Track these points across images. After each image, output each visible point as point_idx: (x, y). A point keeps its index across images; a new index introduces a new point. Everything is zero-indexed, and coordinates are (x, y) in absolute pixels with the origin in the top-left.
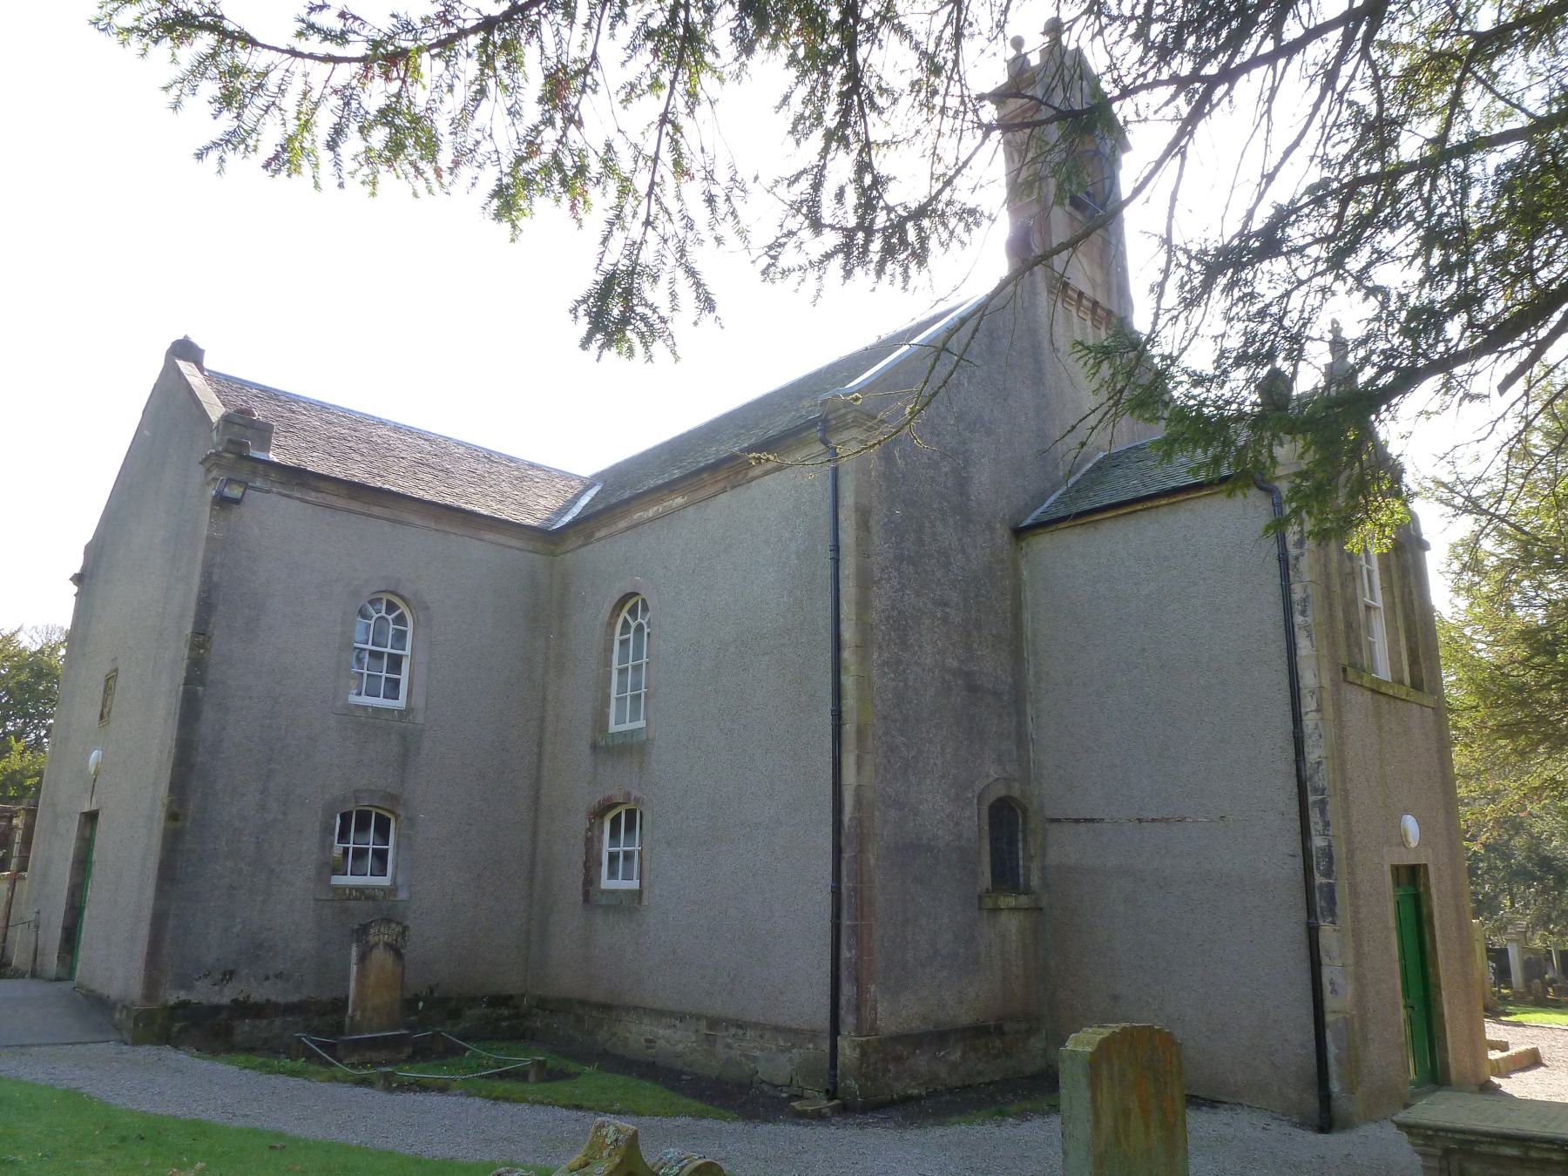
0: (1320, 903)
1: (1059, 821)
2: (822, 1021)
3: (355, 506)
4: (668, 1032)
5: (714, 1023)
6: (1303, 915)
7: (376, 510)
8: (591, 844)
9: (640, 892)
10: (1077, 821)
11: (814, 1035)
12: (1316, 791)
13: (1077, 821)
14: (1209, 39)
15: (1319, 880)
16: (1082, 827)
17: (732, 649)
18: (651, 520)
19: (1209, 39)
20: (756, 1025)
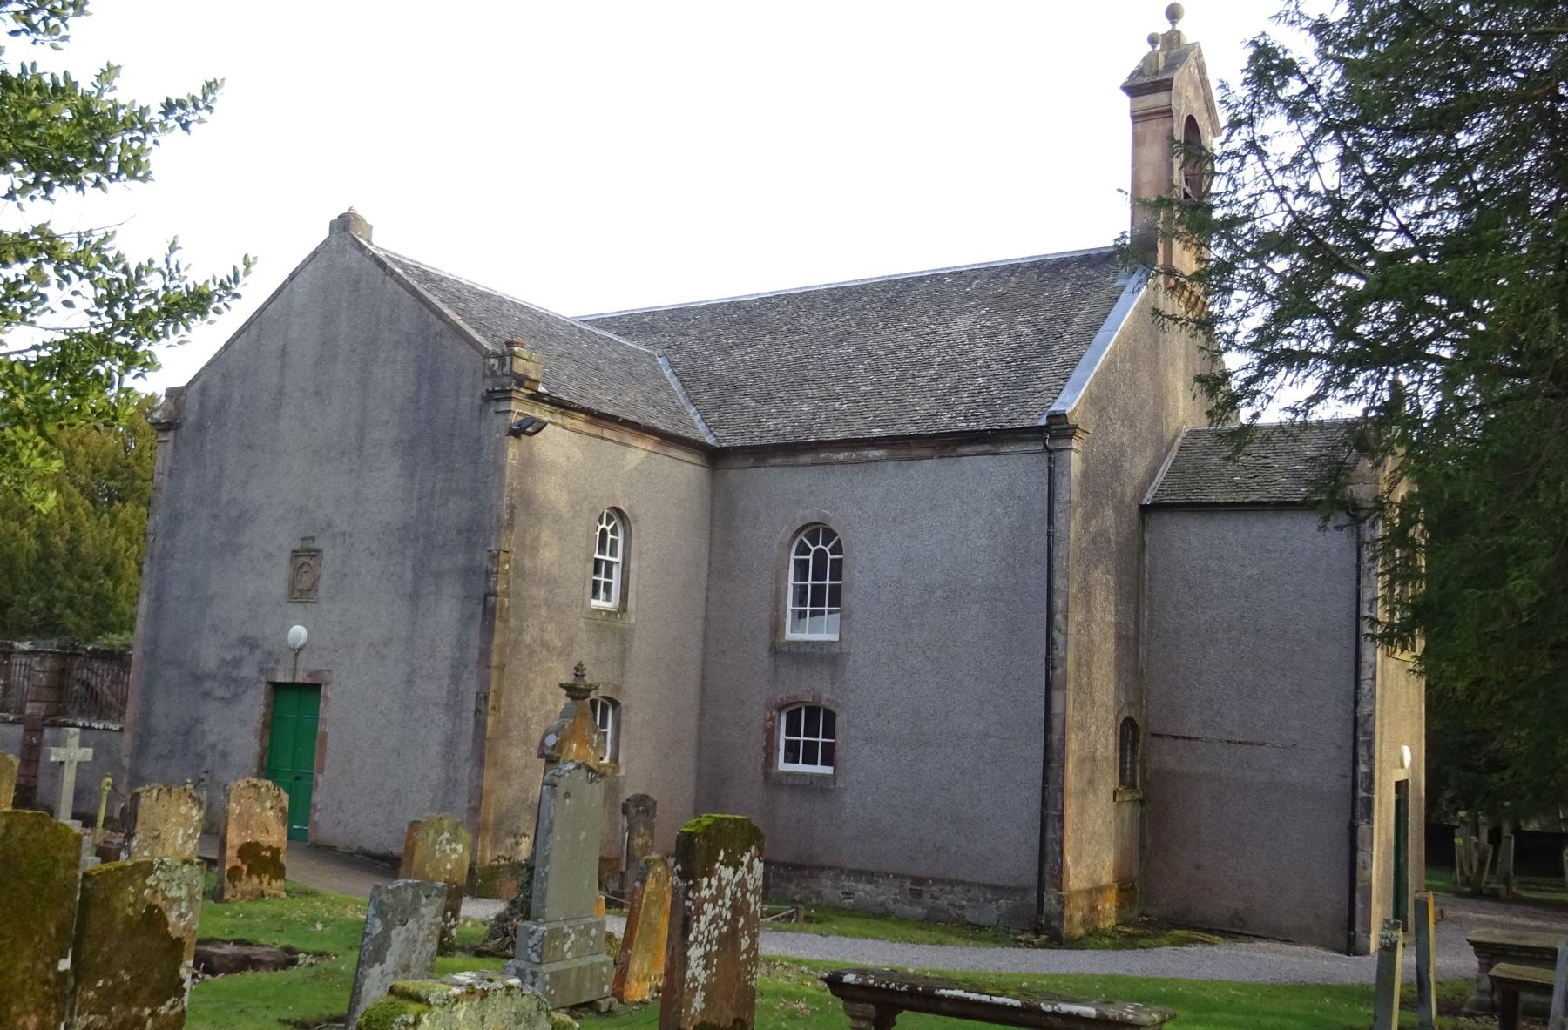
0: (1360, 808)
1: (1161, 736)
2: (1031, 878)
3: (595, 430)
4: (868, 887)
5: (919, 880)
6: (1349, 816)
7: (607, 433)
8: (771, 734)
9: (834, 777)
10: (1176, 738)
11: (1024, 890)
12: (1365, 734)
13: (1176, 738)
14: (1404, 585)
15: (1361, 793)
16: (1180, 742)
17: (939, 593)
18: (842, 463)
19: (1404, 585)
20: (963, 883)
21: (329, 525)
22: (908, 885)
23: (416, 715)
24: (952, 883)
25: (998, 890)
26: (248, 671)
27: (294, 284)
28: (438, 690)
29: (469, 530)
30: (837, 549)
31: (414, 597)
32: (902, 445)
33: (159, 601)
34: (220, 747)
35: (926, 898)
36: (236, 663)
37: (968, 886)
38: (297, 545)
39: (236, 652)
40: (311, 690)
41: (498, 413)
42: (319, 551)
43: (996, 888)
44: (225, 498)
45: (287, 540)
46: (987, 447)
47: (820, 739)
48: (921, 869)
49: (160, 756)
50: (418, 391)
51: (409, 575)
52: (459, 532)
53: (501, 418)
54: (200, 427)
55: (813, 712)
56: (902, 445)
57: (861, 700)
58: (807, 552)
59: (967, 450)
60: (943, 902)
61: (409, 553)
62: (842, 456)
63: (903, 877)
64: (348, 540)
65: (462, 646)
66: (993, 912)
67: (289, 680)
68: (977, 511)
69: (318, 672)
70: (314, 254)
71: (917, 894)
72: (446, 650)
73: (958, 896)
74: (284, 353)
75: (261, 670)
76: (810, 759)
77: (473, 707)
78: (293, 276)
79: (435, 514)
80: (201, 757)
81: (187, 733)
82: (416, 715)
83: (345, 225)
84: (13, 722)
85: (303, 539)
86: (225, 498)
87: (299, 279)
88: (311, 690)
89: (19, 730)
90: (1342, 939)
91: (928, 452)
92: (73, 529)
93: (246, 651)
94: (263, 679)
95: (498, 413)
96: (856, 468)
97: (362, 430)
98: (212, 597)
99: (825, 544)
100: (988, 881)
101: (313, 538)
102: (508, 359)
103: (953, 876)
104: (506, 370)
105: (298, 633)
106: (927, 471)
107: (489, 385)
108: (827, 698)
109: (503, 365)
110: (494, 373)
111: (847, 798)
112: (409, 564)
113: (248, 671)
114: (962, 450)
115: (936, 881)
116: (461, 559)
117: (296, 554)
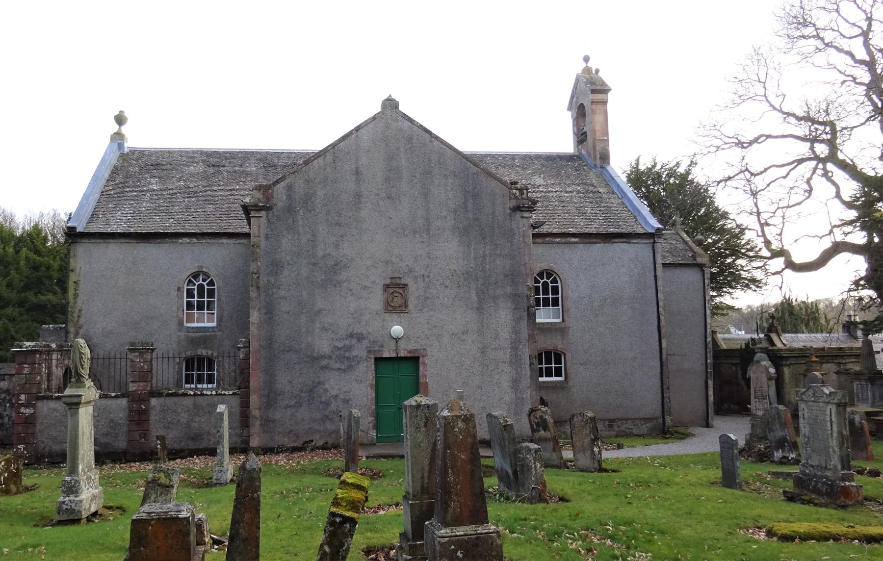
2: (659, 413)
11: (657, 418)
20: (629, 419)
21: (411, 271)
22: (607, 423)
23: (490, 369)
24: (626, 420)
25: (646, 420)
26: (360, 351)
27: (359, 133)
28: (505, 355)
29: (512, 275)
30: (555, 281)
31: (480, 309)
32: (586, 237)
33: (269, 312)
34: (341, 396)
35: (616, 428)
36: (348, 348)
37: (634, 419)
38: (388, 282)
39: (347, 342)
40: (414, 360)
41: (523, 217)
42: (406, 285)
43: (645, 419)
44: (320, 253)
45: (378, 278)
46: (625, 240)
47: (553, 366)
48: (611, 415)
49: (287, 407)
50: (465, 203)
51: (474, 297)
52: (506, 276)
53: (525, 220)
54: (290, 210)
55: (548, 354)
56: (586, 237)
57: (578, 346)
58: (539, 282)
59: (617, 240)
60: (623, 428)
61: (473, 286)
62: (557, 240)
63: (605, 420)
64: (426, 279)
65: (516, 332)
66: (644, 428)
67: (394, 355)
68: (623, 266)
69: (416, 350)
70: (411, 120)
71: (611, 426)
72: (505, 335)
73: (629, 424)
74: (357, 172)
75: (369, 352)
76: (549, 375)
77: (528, 362)
78: (358, 129)
79: (488, 267)
80: (327, 404)
81: (311, 391)
82: (490, 369)
83: (390, 105)
84: (115, 397)
85: (392, 278)
86: (320, 253)
87: (363, 131)
88: (414, 360)
89: (124, 402)
90: (704, 423)
91: (598, 240)
92: (754, 281)
93: (354, 341)
94: (372, 356)
95: (523, 217)
96: (565, 246)
97: (428, 220)
98: (319, 311)
99: (551, 282)
100: (642, 416)
101: (400, 278)
102: (525, 191)
103: (626, 417)
104: (524, 196)
105: (397, 330)
106: (599, 248)
107: (513, 203)
108: (560, 347)
109: (522, 194)
110: (516, 198)
111: (574, 390)
112: (474, 292)
113: (360, 351)
114: (614, 241)
115: (619, 420)
116: (509, 289)
117: (387, 286)
